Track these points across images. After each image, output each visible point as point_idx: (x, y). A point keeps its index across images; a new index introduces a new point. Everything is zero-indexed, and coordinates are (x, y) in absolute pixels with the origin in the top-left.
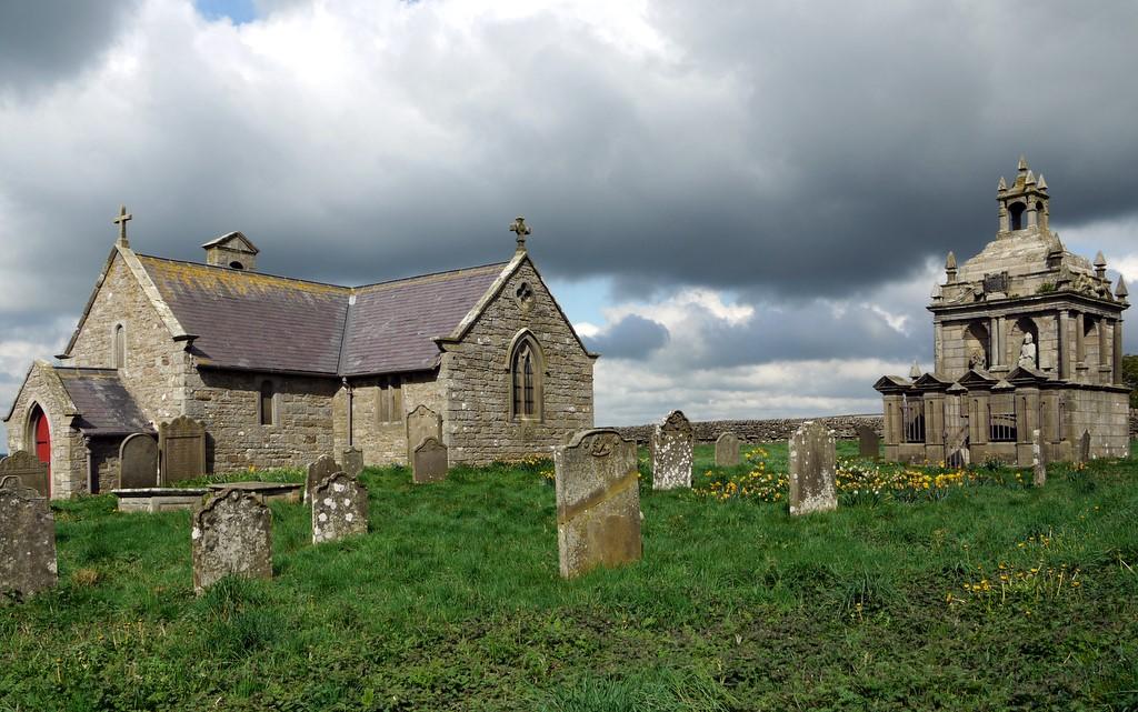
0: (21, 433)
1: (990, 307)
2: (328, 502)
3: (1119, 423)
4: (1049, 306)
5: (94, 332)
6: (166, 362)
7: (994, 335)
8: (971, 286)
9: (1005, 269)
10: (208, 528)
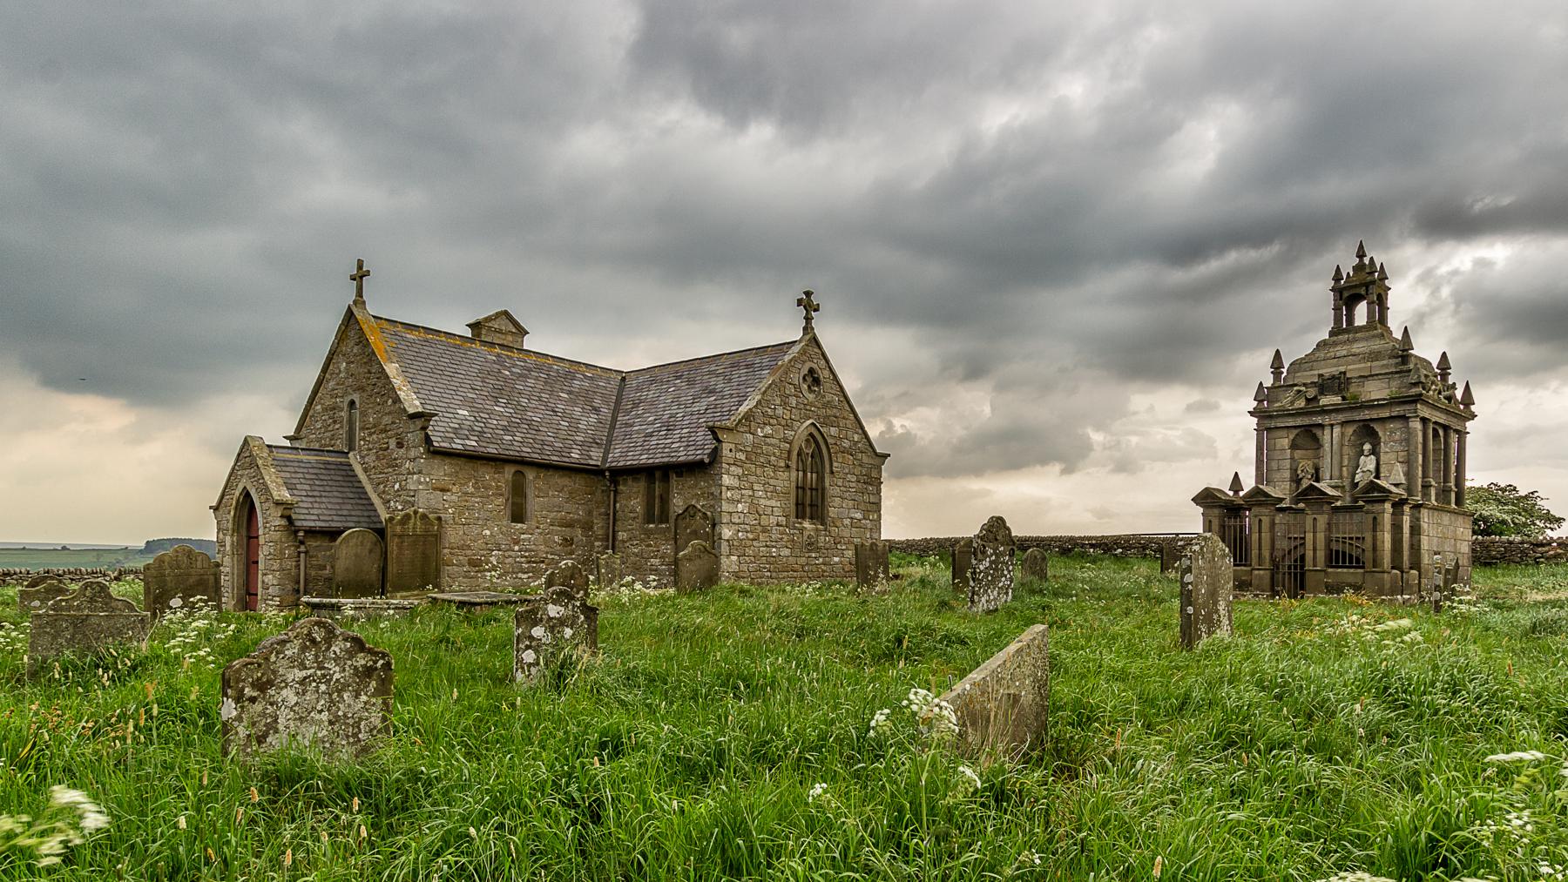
0: (230, 526)
1: (1324, 411)
2: (538, 632)
3: (1462, 551)
4: (1397, 411)
5: (325, 410)
6: (400, 445)
7: (1327, 446)
8: (1303, 388)
9: (1342, 369)
10: (253, 700)
